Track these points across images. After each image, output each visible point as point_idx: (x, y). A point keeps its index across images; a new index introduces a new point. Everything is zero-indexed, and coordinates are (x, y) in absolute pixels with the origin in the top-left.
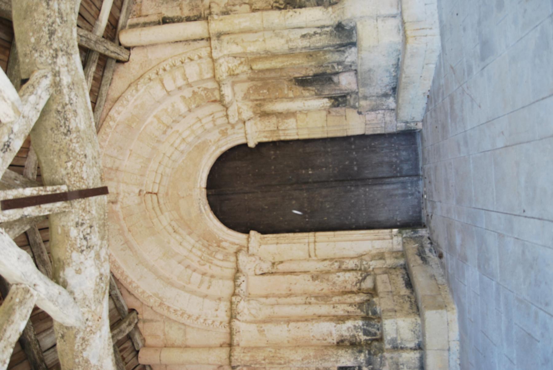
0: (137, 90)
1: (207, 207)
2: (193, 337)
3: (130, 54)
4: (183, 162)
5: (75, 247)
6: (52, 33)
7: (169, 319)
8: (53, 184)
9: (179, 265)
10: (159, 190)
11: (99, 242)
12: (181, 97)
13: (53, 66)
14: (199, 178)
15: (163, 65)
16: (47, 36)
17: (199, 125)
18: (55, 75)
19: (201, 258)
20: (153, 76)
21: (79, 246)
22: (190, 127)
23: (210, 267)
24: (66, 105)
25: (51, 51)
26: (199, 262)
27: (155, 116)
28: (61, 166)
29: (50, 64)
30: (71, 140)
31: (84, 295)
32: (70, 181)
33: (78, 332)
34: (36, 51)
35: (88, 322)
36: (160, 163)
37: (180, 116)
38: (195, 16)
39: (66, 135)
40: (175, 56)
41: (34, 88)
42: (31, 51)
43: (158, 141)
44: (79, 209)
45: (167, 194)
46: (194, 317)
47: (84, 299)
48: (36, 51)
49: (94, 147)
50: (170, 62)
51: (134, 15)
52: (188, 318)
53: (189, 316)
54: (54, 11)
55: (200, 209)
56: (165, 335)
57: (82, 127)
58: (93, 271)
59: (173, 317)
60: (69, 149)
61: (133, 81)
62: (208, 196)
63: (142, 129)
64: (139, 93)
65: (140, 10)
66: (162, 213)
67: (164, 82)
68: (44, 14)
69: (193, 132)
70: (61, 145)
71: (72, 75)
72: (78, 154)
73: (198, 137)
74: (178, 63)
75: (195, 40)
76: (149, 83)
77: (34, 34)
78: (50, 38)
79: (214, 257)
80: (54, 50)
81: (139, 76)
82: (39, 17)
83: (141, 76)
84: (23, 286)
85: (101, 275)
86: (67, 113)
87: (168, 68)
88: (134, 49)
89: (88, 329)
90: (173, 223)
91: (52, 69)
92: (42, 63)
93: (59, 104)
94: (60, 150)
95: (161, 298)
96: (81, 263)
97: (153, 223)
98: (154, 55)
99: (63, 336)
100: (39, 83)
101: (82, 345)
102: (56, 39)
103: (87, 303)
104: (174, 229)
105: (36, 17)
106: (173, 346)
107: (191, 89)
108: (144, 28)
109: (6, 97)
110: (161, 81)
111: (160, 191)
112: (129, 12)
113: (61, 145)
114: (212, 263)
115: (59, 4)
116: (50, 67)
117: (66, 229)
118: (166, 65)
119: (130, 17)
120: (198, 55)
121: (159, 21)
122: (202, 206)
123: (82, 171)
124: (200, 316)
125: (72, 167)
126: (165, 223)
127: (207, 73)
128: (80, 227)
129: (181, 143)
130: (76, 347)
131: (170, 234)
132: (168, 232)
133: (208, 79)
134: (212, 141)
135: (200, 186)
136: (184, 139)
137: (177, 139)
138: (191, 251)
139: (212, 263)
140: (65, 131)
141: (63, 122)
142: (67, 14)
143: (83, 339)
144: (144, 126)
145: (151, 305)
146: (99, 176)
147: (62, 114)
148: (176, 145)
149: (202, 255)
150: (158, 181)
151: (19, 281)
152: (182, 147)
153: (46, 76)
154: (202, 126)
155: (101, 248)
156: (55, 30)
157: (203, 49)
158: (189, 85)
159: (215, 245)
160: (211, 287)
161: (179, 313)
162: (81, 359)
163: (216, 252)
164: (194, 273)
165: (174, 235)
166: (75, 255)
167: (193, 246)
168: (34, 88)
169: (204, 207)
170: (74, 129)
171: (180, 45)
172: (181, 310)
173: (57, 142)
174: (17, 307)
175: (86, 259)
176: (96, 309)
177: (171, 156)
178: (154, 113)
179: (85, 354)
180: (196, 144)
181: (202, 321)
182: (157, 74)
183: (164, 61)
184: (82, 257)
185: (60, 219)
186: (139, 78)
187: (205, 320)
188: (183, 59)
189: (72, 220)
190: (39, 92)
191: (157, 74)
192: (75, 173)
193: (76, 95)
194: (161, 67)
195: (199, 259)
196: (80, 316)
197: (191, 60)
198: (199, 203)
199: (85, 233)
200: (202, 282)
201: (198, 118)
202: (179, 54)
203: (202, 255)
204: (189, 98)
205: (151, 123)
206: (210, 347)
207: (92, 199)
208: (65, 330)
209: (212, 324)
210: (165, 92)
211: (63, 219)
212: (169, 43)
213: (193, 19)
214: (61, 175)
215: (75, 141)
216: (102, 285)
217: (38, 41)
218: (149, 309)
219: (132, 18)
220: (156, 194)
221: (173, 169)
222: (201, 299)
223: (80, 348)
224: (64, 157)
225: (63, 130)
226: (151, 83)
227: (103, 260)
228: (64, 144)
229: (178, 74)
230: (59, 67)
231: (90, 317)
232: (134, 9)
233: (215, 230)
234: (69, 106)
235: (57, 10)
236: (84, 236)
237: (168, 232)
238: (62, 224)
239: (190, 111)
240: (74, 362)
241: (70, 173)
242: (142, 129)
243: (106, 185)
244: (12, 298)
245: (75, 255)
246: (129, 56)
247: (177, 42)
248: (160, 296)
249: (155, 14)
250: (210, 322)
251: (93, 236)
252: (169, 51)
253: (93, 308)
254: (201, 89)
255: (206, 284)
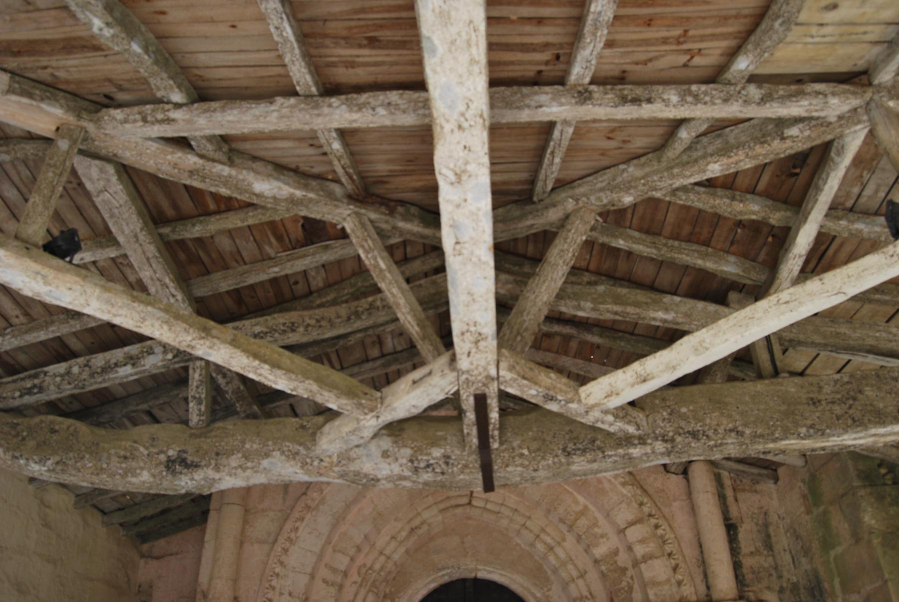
0: (624, 484)
1: (446, 579)
2: (255, 553)
3: (677, 474)
4: (518, 544)
5: (418, 453)
6: (694, 435)
7: (285, 520)
8: (502, 428)
9: (362, 536)
10: (476, 507)
11: (421, 480)
12: (617, 548)
13: (652, 435)
14: (490, 569)
15: (665, 526)
16: (690, 429)
17: (575, 574)
18: (640, 438)
19: (370, 568)
20: (646, 509)
21: (420, 458)
22: (571, 560)
23: (355, 583)
24: (603, 452)
25: (671, 434)
26: (365, 565)
27: (586, 507)
28: (523, 441)
29: (654, 432)
30: (557, 456)
31: (354, 459)
32: (503, 451)
33: (308, 449)
34: (670, 414)
35: (318, 461)
36: (516, 510)
37: (588, 546)
38: (744, 576)
39: (564, 450)
40: (679, 545)
41: (623, 418)
42: (669, 407)
43: (548, 511)
44: (467, 460)
45: (469, 518)
46: (283, 558)
47: (349, 459)
48: (670, 414)
49: (548, 478)
50: (670, 536)
51: (735, 481)
52: (283, 549)
53: (286, 551)
54: (723, 438)
55: (443, 569)
56: (263, 510)
57: (574, 468)
58: (384, 472)
59: (288, 526)
60: (545, 452)
61: (638, 478)
62: (463, 581)
63: (566, 487)
64: (620, 487)
65: (744, 490)
66: (442, 511)
67: (638, 525)
68: (718, 425)
69: (564, 564)
70: (551, 442)
71: (641, 457)
72: (539, 462)
73: (555, 571)
74: (668, 548)
75: (706, 575)
76: (636, 501)
77: (692, 411)
78: (688, 432)
79: (369, 591)
80: (673, 437)
81: (645, 487)
82: (712, 419)
83: (645, 491)
84: (379, 406)
85: (378, 480)
86: (593, 453)
87: (660, 532)
88: (684, 480)
89: (308, 460)
90: (425, 528)
91: (649, 435)
92: (655, 421)
93: (604, 442)
94: (544, 440)
95: (317, 508)
96: (397, 459)
97: (427, 496)
98: (678, 511)
99: (303, 427)
100: (629, 422)
101: (290, 451)
102: (687, 441)
103: (343, 462)
104: (416, 528)
105: (714, 415)
106: (245, 522)
107: (630, 566)
108: (717, 497)
109: (610, 399)
110: (639, 521)
111: (473, 509)
112: (739, 473)
113: (551, 442)
114: (361, 586)
115: (733, 443)
116: (650, 432)
117: (442, 442)
118: (664, 530)
119: (732, 475)
120: (683, 581)
121: (731, 519)
122: (449, 571)
123: (517, 466)
124: (285, 567)
125: (522, 455)
126: (426, 515)
127: (656, 594)
128: (443, 460)
129: (545, 544)
130: (287, 444)
131: (409, 522)
132: (411, 520)
133: (647, 595)
134: (550, 593)
135: (480, 570)
136: (551, 549)
137: (553, 538)
138: (381, 553)
139: (361, 586)
140: (569, 449)
141: (580, 446)
142: (722, 451)
143: (297, 453)
144: (571, 490)
145: (309, 493)
146: (509, 483)
147: (590, 446)
148: (542, 536)
149: (374, 571)
150: (489, 506)
151: (387, 402)
152: (540, 546)
153: (638, 429)
154: (573, 580)
155: (414, 482)
156: (699, 440)
157: (693, 590)
158: (636, 564)
159: (387, 591)
160: (325, 585)
161: (293, 535)
162: (271, 448)
163: (377, 594)
164: (348, 559)
165: (407, 528)
166: (407, 452)
167: (388, 558)
168: (623, 418)
169: (447, 574)
170: (571, 460)
171: (697, 552)
172: (297, 538)
173: (554, 437)
174: (355, 401)
175: (401, 466)
176: (333, 471)
177: (527, 528)
178: (591, 507)
179: (277, 454)
180: (545, 567)
181: (277, 570)
182: (650, 515)
183: (670, 526)
184: (404, 461)
185: (455, 435)
186: (642, 487)
187: (278, 575)
188: (676, 557)
189: (453, 452)
190: (618, 424)
191: (650, 515)
192: (513, 458)
193: (616, 462)
194: (661, 522)
195: (368, 565)
196: (328, 453)
197: (675, 569)
198: (453, 567)
199: (435, 466)
200: (334, 570)
201: (586, 572)
202: (682, 551)
203: (374, 571)
204: (616, 562)
205: (576, 502)
206: (235, 581)
207: (480, 476)
208: (310, 431)
209: (271, 586)
210: (623, 526)
211: (455, 438)
212: (699, 534)
213: (738, 572)
214: (511, 439)
215: (556, 460)
216: (365, 481)
217: (684, 417)
218: (304, 490)
219: (731, 478)
220: (470, 503)
221: (507, 529)
222: (309, 570)
223: (285, 449)
224: (535, 445)
225: (571, 446)
226: (636, 506)
227: (398, 483)
228: (552, 446)
229: (651, 547)
230: (651, 444)
231: (323, 464)
232: (744, 481)
233: (410, 592)
234: (601, 455)
235: (725, 441)
236: (432, 464)
237: (411, 520)
238: (449, 437)
239: (596, 562)
240: (268, 440)
241: (513, 452)
242: (566, 487)
243: (496, 490)
244: (366, 394)
245: (407, 452)
246: (674, 473)
247: (701, 546)
248: (321, 507)
249: (740, 513)
250: (274, 583)
251: (430, 475)
252: (686, 533)
253: (336, 469)
254: (630, 581)
255: (330, 577)
